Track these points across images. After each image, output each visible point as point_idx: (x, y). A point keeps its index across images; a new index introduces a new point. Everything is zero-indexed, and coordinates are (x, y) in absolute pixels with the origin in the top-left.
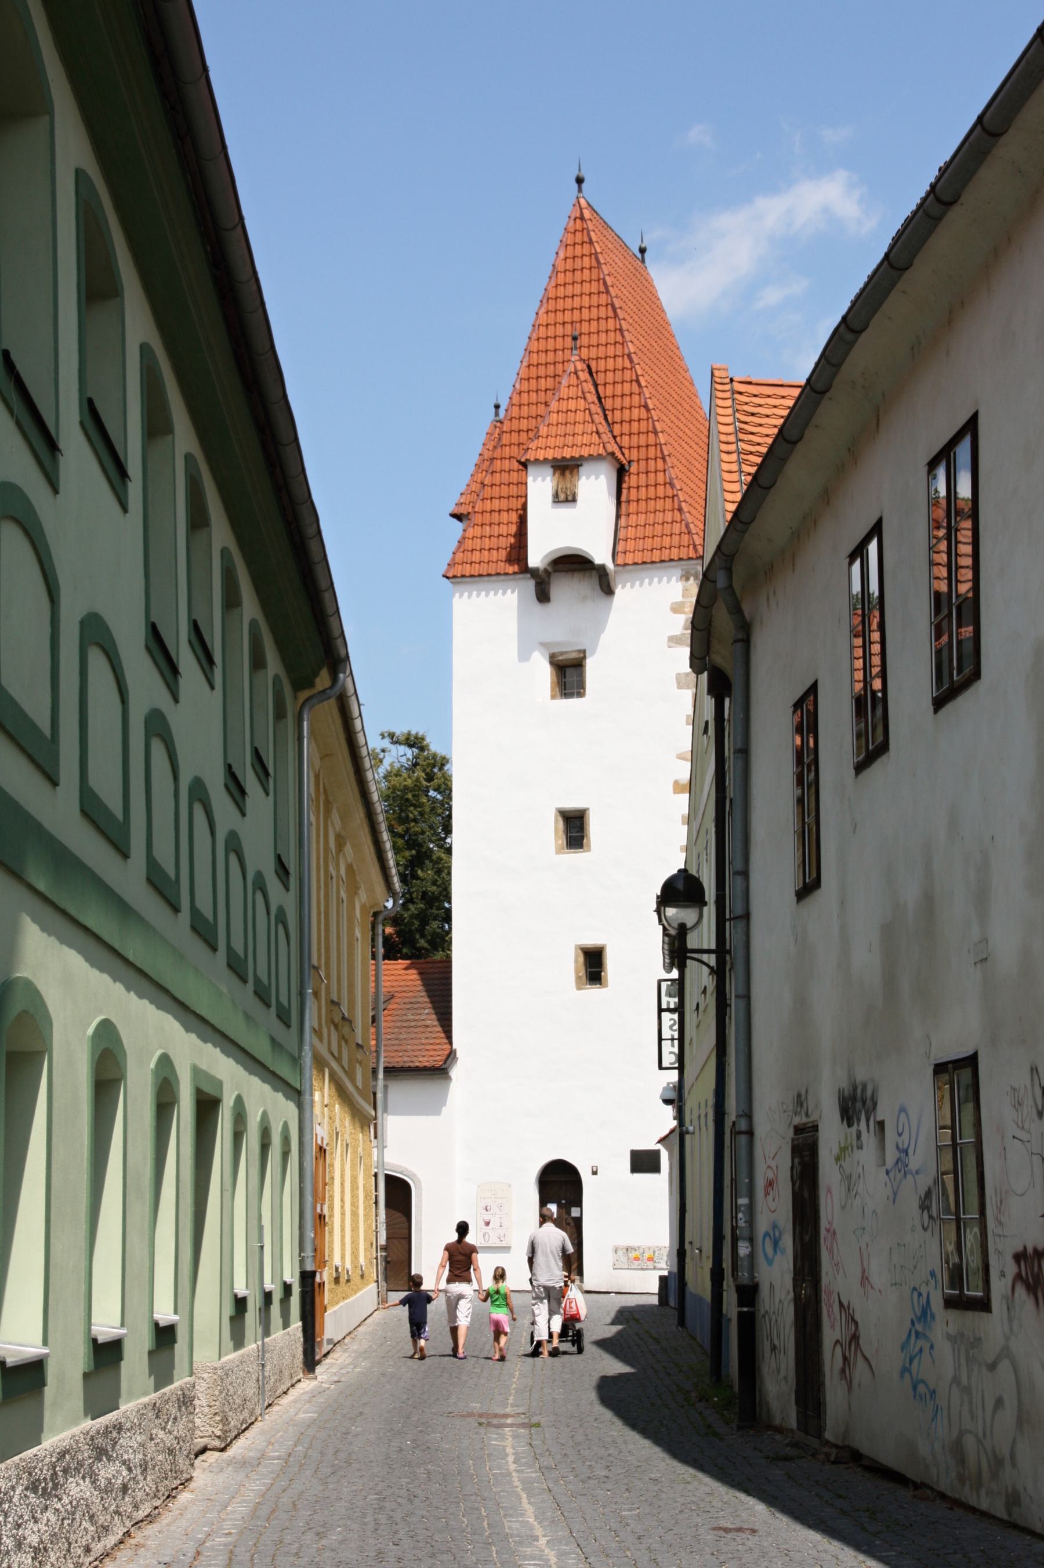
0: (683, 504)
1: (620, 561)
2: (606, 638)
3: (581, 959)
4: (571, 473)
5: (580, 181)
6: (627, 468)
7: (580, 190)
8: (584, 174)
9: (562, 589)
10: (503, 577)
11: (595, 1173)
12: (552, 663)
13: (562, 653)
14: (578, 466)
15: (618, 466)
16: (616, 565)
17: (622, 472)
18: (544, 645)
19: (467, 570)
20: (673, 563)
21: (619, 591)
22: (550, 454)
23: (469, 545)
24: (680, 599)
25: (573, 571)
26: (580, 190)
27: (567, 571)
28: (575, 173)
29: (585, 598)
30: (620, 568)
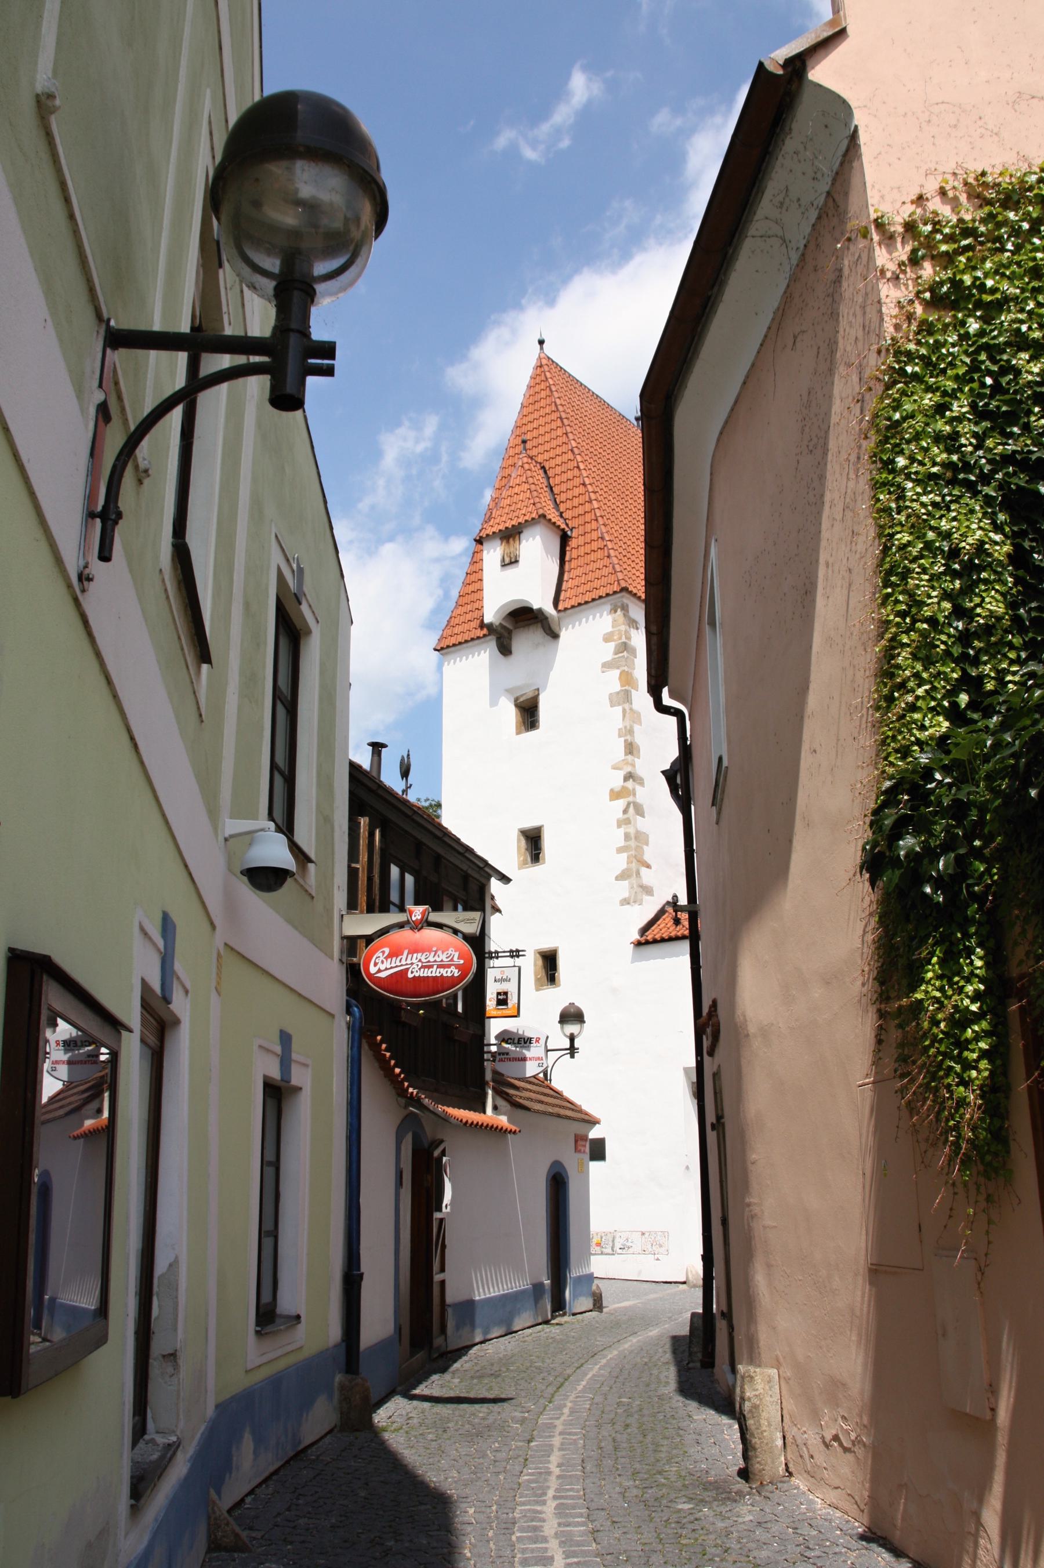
0: (611, 551)
1: (560, 607)
2: (555, 675)
3: (540, 962)
4: (514, 540)
5: (541, 342)
6: (569, 533)
7: (542, 348)
8: (544, 337)
9: (524, 642)
10: (477, 642)
11: (687, 1168)
12: (516, 706)
13: (522, 695)
14: (520, 533)
15: (561, 533)
16: (559, 611)
17: (565, 539)
18: (508, 691)
19: (453, 640)
20: (602, 600)
21: (563, 634)
22: (496, 529)
23: (454, 622)
24: (610, 629)
25: (528, 625)
26: (542, 348)
27: (524, 627)
28: (538, 337)
29: (537, 645)
30: (562, 614)
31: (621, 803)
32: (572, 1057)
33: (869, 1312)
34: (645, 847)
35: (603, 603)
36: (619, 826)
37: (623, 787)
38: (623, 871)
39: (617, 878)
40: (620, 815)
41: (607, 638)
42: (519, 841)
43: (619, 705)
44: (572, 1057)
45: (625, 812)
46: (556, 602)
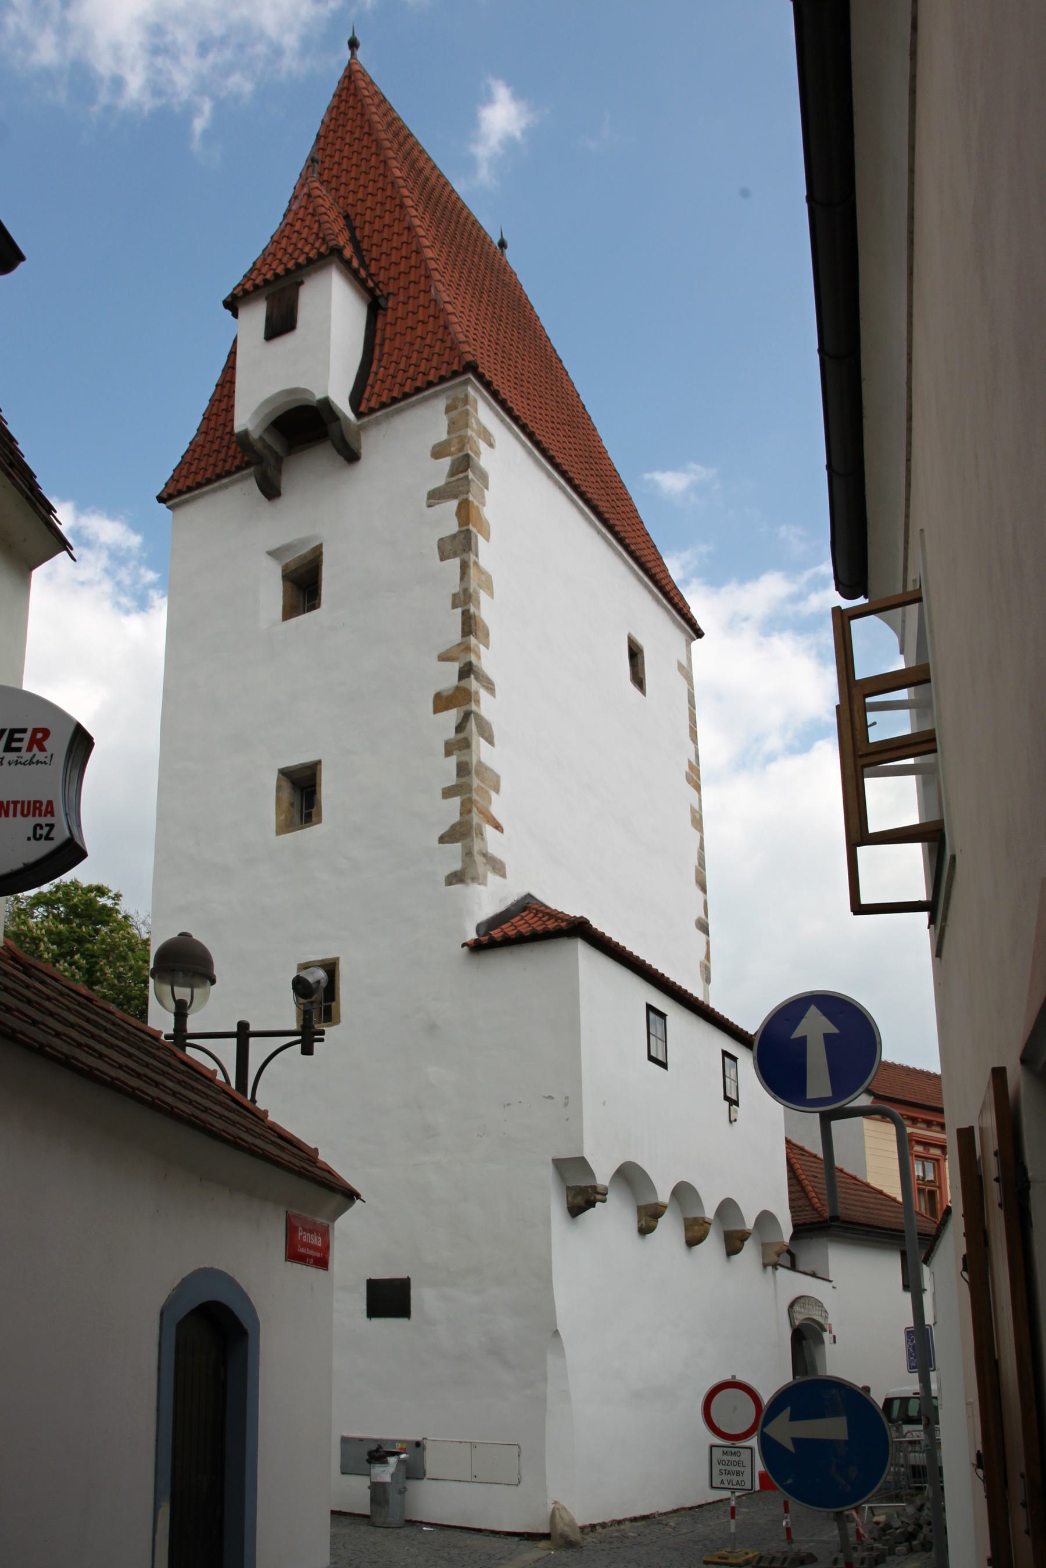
1: (363, 408)
5: (353, 44)
24: (444, 437)
31: (451, 717)
32: (307, 1051)
33: (228, 1134)
34: (493, 794)
35: (435, 395)
36: (448, 753)
37: (457, 688)
38: (453, 827)
39: (442, 840)
40: (451, 734)
41: (438, 452)
42: (279, 788)
43: (455, 555)
44: (307, 1051)
45: (460, 728)
46: (356, 399)
